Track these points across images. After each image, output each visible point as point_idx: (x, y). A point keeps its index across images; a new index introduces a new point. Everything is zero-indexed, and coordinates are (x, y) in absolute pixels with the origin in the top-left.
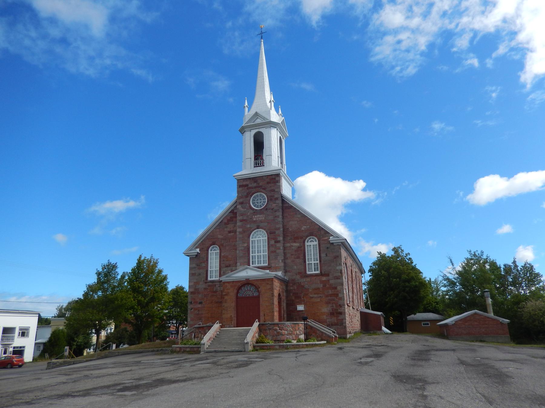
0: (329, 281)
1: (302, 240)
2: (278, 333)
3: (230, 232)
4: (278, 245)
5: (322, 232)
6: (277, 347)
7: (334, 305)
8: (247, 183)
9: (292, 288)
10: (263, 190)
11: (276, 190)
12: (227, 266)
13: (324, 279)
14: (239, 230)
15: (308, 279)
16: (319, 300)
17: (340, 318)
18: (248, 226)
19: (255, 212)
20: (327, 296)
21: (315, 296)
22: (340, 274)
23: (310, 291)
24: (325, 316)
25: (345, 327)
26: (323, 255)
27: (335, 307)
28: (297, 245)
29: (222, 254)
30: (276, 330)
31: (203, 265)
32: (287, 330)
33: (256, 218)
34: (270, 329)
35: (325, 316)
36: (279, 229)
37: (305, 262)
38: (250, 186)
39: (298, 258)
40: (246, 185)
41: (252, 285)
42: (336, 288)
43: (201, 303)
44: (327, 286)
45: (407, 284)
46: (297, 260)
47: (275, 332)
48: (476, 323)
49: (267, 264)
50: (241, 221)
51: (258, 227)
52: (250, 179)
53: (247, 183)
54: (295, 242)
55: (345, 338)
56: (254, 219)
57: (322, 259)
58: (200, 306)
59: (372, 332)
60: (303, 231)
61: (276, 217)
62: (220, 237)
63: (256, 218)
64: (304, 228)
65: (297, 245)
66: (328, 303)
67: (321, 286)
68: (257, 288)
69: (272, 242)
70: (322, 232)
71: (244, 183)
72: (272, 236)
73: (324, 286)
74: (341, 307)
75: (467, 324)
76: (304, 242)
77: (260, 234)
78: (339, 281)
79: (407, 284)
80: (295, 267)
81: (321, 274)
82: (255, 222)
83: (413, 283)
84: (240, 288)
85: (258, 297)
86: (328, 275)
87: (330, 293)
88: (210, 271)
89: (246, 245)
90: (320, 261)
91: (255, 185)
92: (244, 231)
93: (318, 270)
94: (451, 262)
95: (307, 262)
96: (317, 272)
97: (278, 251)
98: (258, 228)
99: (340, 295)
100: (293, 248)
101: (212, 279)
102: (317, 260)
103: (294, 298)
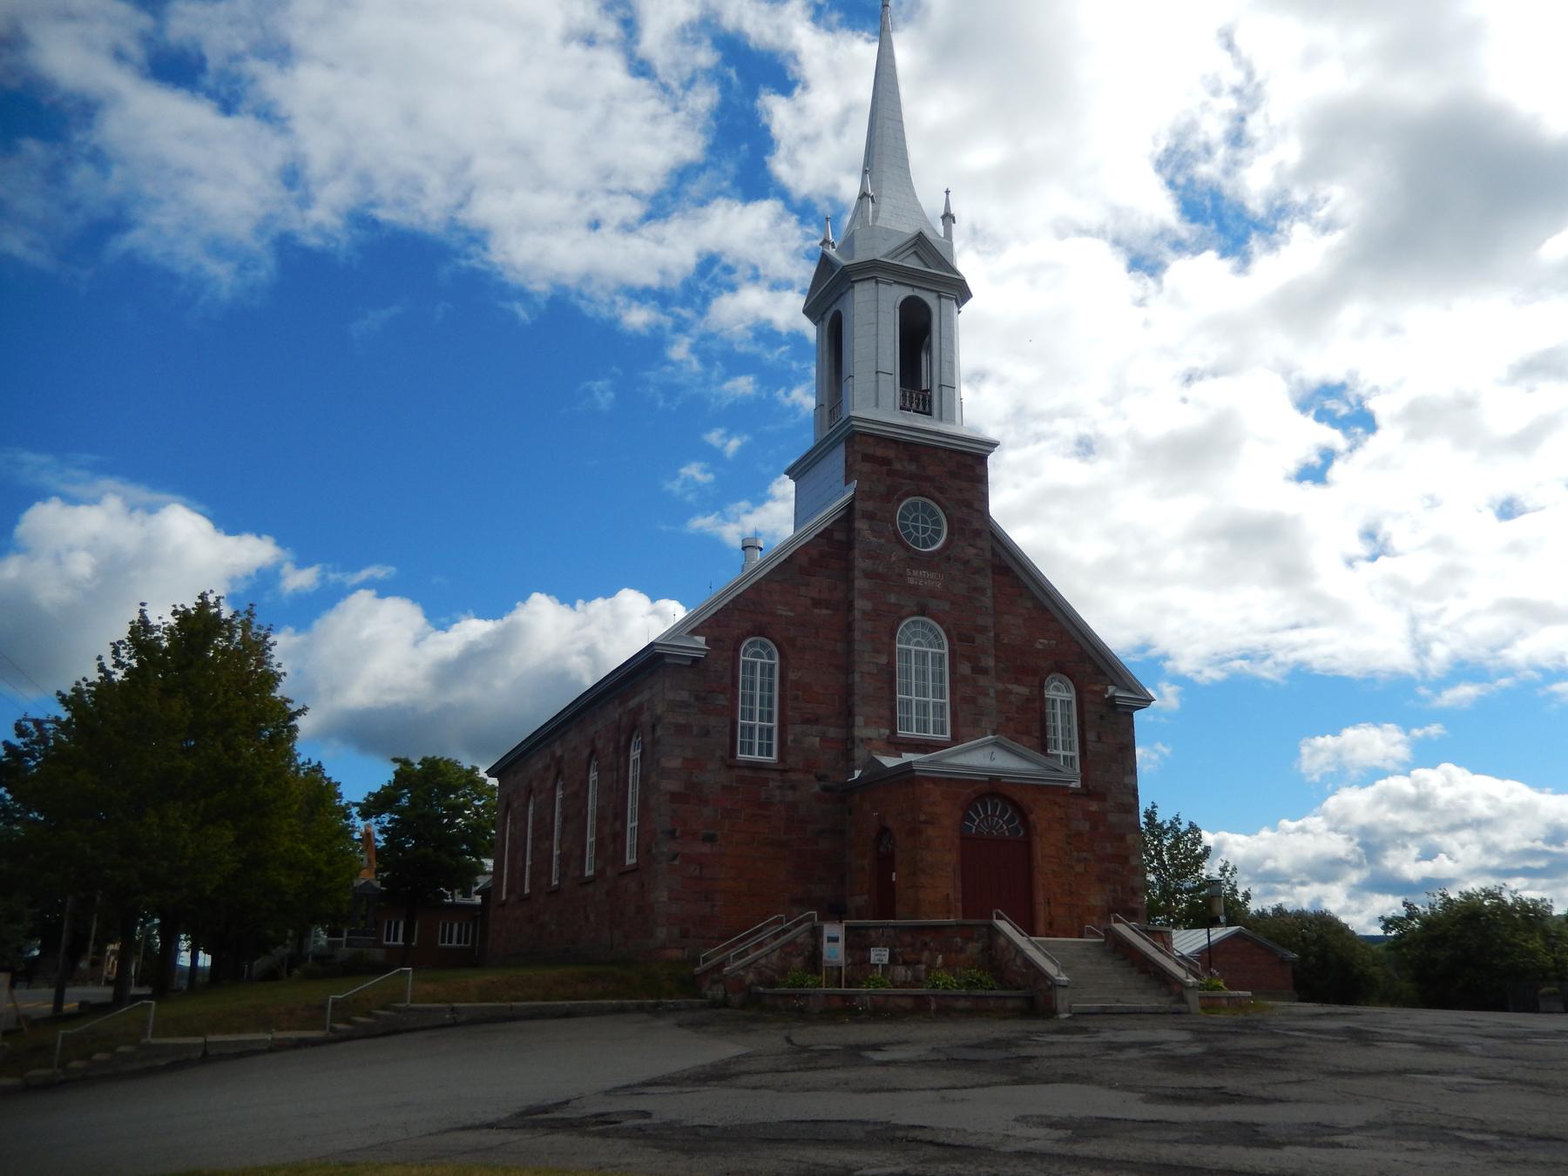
3: (817, 603)
4: (982, 681)
6: (1224, 1002)
8: (891, 454)
10: (937, 495)
11: (976, 505)
12: (806, 721)
13: (1094, 807)
14: (860, 604)
18: (893, 599)
19: (917, 560)
26: (1091, 736)
29: (792, 676)
31: (722, 700)
33: (916, 577)
36: (982, 630)
38: (897, 466)
40: (885, 462)
41: (1008, 800)
42: (1122, 838)
43: (710, 839)
50: (868, 575)
51: (923, 611)
54: (1017, 681)
56: (911, 581)
57: (1090, 746)
58: (705, 849)
61: (975, 589)
62: (782, 611)
63: (916, 577)
64: (1041, 643)
67: (1086, 827)
68: (1021, 812)
69: (965, 668)
71: (879, 452)
72: (963, 643)
76: (1042, 687)
77: (924, 636)
82: (914, 590)
85: (1028, 844)
86: (1101, 797)
88: (743, 727)
89: (884, 660)
90: (734, 723)
93: (769, 754)
96: (765, 758)
97: (981, 700)
98: (923, 614)
101: (746, 757)
102: (770, 721)
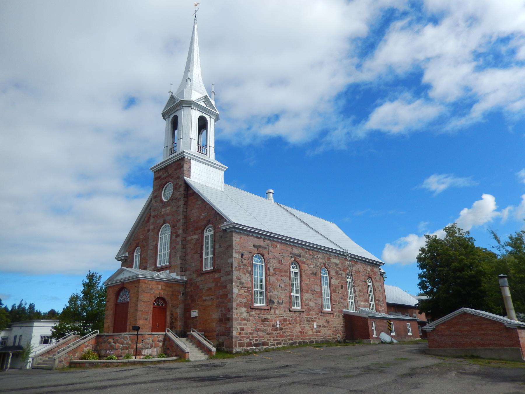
0: (220, 278)
1: (199, 231)
2: (111, 346)
5: (218, 218)
6: (87, 365)
7: (223, 309)
9: (189, 290)
13: (216, 276)
15: (203, 278)
16: (210, 303)
17: (228, 326)
20: (218, 298)
21: (208, 298)
22: (230, 269)
23: (204, 292)
24: (214, 324)
25: (232, 337)
26: (217, 246)
27: (224, 312)
28: (196, 237)
29: (142, 256)
30: (109, 343)
32: (122, 343)
34: (105, 342)
35: (214, 324)
37: (201, 256)
38: (163, 177)
39: (196, 253)
42: (225, 287)
44: (219, 284)
45: (458, 274)
46: (195, 255)
47: (109, 346)
48: (466, 328)
49: (167, 263)
52: (162, 169)
53: (161, 174)
54: (195, 234)
55: (231, 353)
57: (216, 251)
59: (357, 341)
60: (202, 219)
65: (196, 237)
66: (218, 307)
67: (213, 285)
69: (174, 237)
70: (218, 218)
73: (216, 285)
74: (229, 311)
75: (452, 329)
76: (202, 233)
78: (229, 277)
79: (458, 274)
80: (193, 264)
81: (214, 271)
83: (467, 273)
84: (118, 294)
87: (221, 293)
91: (166, 175)
92: (155, 228)
94: (496, 237)
95: (204, 257)
99: (229, 296)
100: (193, 241)
103: (190, 302)
